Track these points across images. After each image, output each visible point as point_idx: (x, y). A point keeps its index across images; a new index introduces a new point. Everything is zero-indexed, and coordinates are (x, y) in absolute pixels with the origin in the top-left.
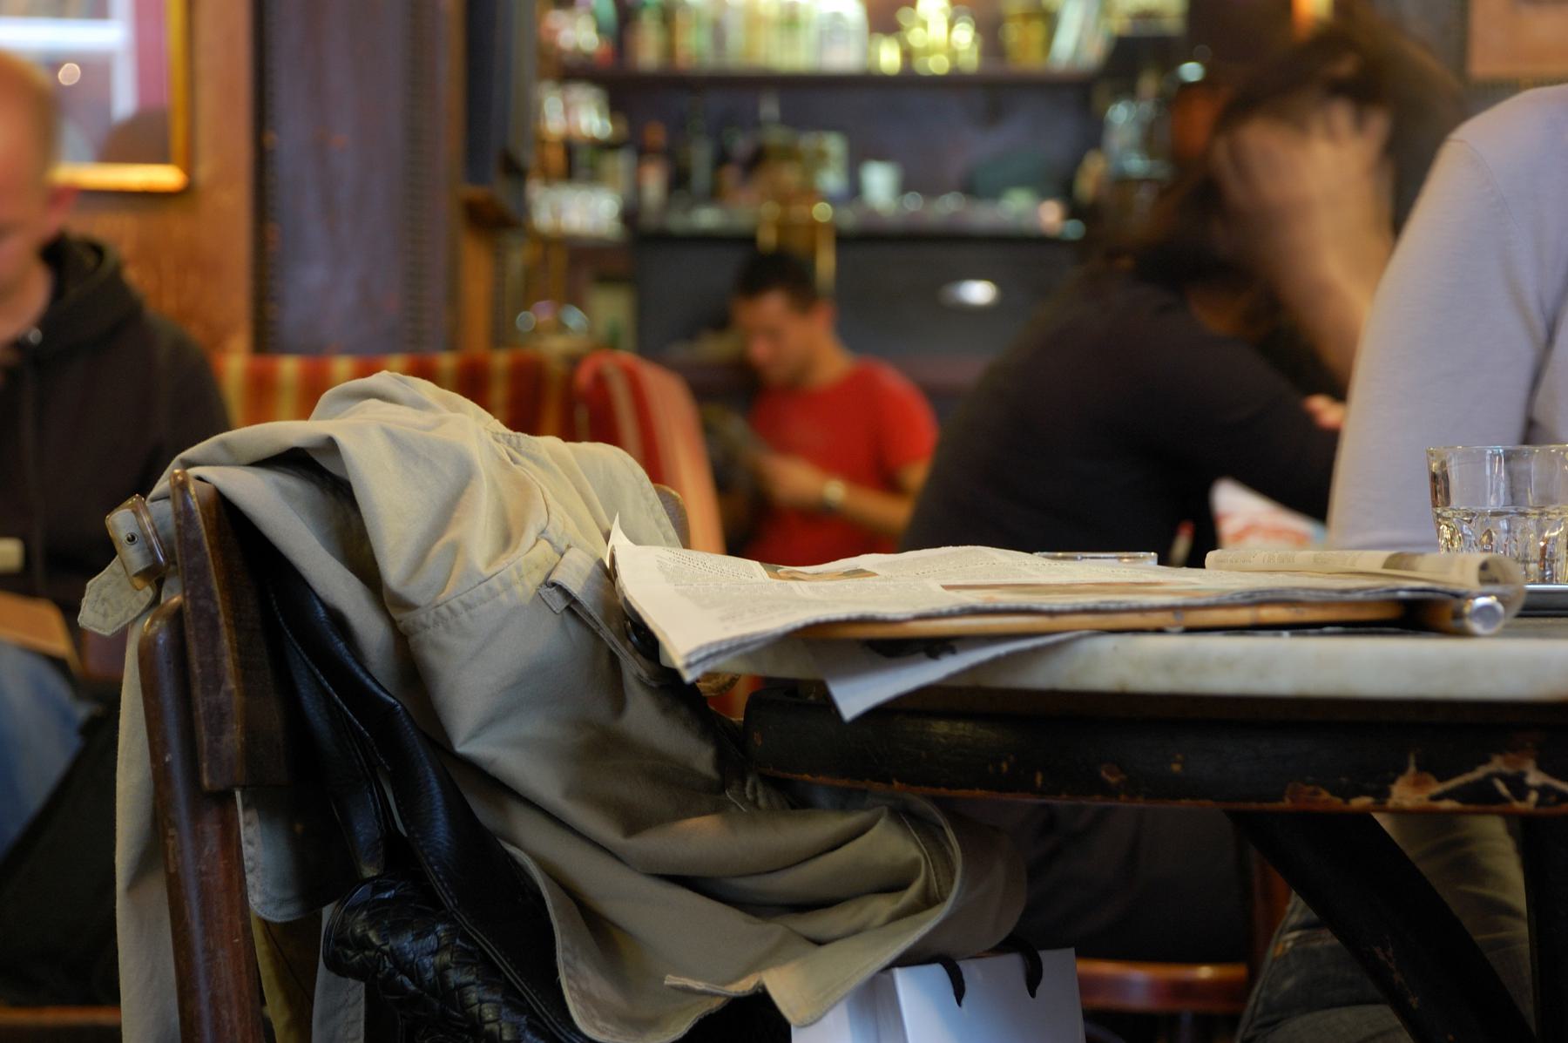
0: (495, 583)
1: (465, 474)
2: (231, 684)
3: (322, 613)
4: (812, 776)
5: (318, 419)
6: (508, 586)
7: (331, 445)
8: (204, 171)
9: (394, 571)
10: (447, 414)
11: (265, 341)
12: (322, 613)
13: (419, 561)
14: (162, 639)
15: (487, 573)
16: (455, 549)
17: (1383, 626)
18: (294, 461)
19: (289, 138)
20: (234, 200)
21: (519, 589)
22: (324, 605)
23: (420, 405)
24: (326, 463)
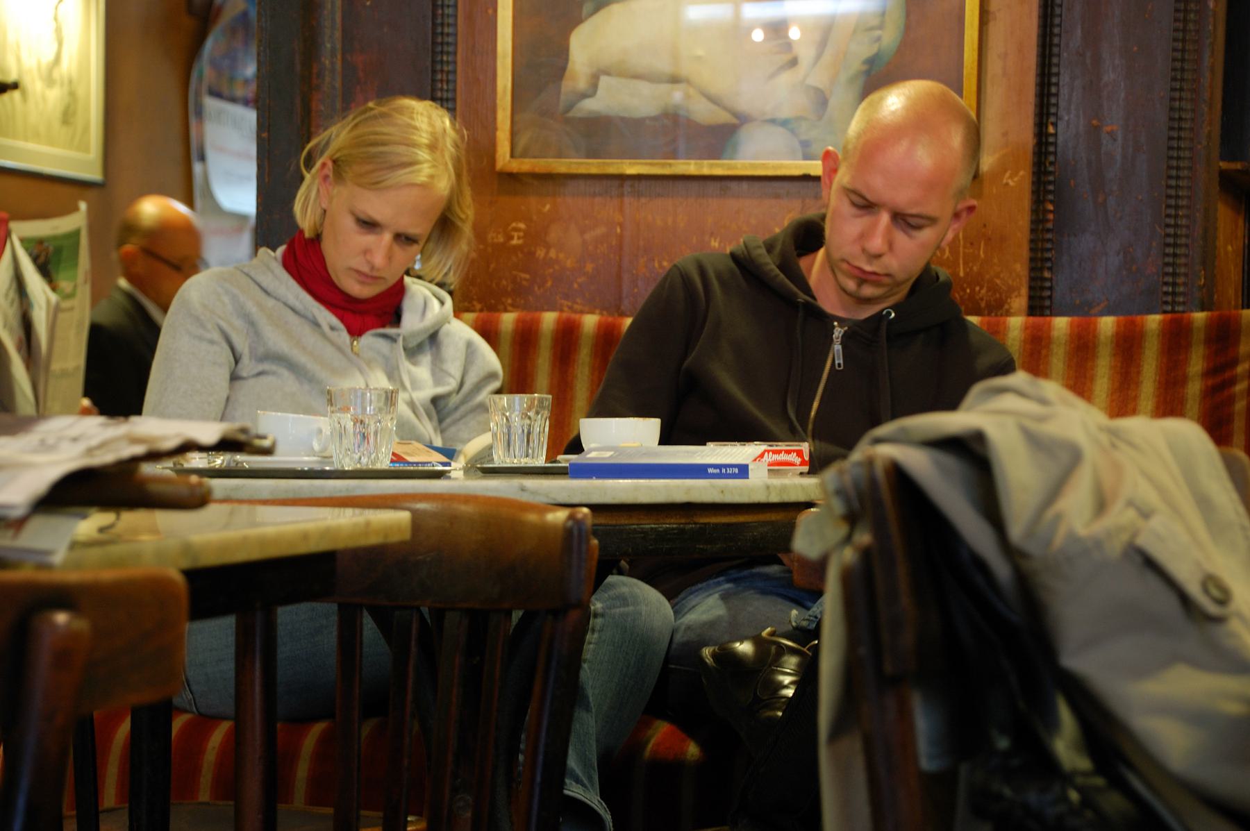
9: (1016, 531)
11: (1039, 306)
16: (1058, 518)
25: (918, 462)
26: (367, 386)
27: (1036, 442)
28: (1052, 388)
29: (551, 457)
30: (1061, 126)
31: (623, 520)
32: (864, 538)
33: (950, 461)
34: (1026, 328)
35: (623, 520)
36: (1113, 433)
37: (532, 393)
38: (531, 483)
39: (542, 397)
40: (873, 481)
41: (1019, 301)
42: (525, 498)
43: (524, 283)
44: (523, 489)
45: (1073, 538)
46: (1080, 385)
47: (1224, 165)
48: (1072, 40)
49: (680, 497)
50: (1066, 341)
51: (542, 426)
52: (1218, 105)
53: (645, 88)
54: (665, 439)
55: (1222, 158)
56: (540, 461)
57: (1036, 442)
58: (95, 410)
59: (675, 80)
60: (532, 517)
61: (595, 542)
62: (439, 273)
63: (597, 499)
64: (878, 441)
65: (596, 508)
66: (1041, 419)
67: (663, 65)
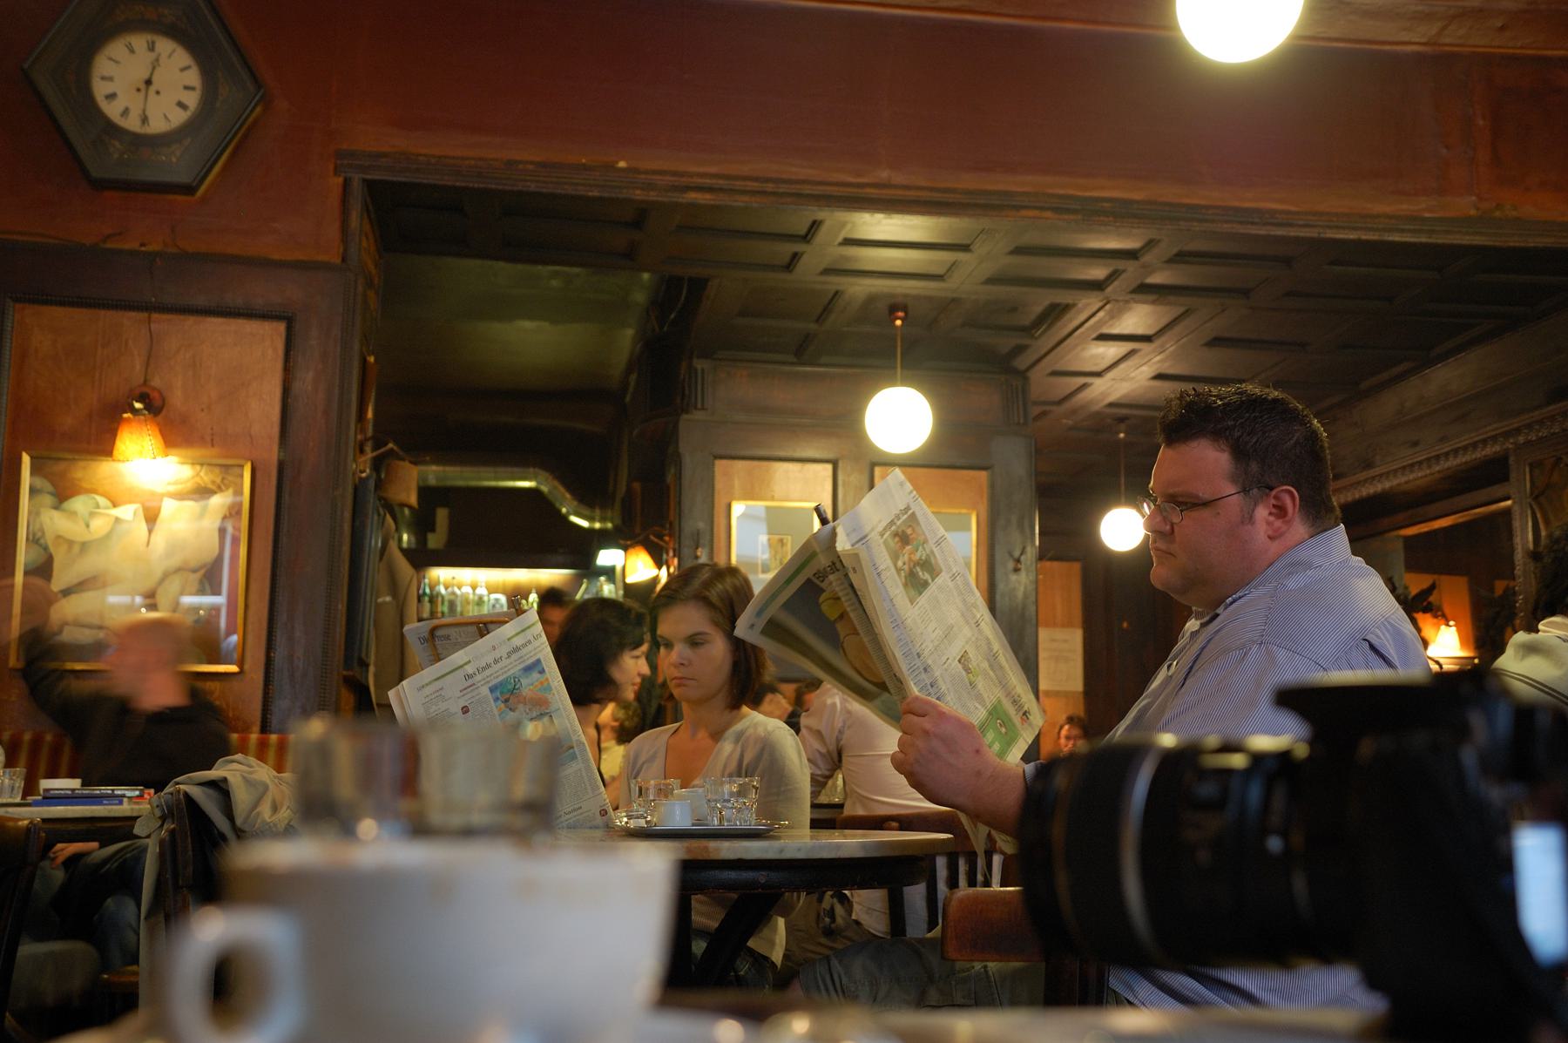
0: (271, 824)
1: (266, 788)
2: (190, 853)
3: (216, 832)
4: (957, 814)
5: (216, 770)
6: (275, 825)
7: (225, 780)
8: (246, 667)
9: (239, 821)
10: (257, 769)
11: (265, 728)
12: (216, 832)
13: (248, 817)
14: (167, 839)
15: (269, 820)
16: (258, 814)
17: (976, 868)
18: (213, 784)
19: (280, 654)
20: (256, 676)
21: (279, 826)
22: (218, 830)
23: (466, 701)
24: (221, 784)
25: (196, 792)
26: (145, 381)
27: (248, 782)
28: (252, 760)
29: (23, 797)
30: (277, 653)
31: (58, 826)
32: (169, 826)
33: (210, 791)
34: (258, 739)
35: (58, 826)
36: (279, 779)
37: (16, 767)
38: (11, 810)
39: (20, 770)
40: (178, 800)
41: (256, 728)
42: (8, 815)
43: (1033, 332)
44: (7, 812)
45: (264, 821)
46: (261, 756)
47: (345, 673)
48: (282, 617)
49: (88, 814)
50: (725, 740)
51: (20, 784)
52: (343, 647)
53: (87, 632)
54: (83, 785)
55: (344, 670)
56: (18, 800)
57: (248, 782)
58: (556, 631)
59: (100, 628)
60: (11, 824)
61: (44, 835)
62: (545, 177)
63: (46, 816)
64: (178, 783)
65: (44, 820)
66: (251, 773)
67: (96, 621)
